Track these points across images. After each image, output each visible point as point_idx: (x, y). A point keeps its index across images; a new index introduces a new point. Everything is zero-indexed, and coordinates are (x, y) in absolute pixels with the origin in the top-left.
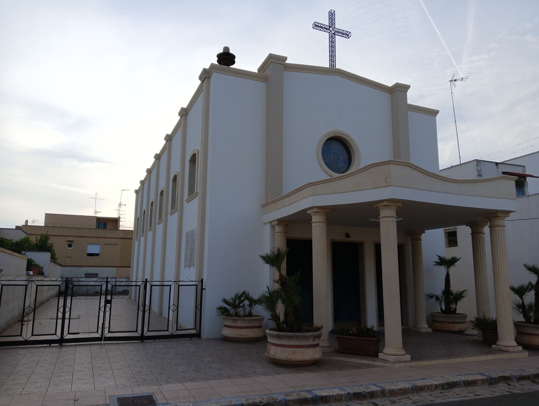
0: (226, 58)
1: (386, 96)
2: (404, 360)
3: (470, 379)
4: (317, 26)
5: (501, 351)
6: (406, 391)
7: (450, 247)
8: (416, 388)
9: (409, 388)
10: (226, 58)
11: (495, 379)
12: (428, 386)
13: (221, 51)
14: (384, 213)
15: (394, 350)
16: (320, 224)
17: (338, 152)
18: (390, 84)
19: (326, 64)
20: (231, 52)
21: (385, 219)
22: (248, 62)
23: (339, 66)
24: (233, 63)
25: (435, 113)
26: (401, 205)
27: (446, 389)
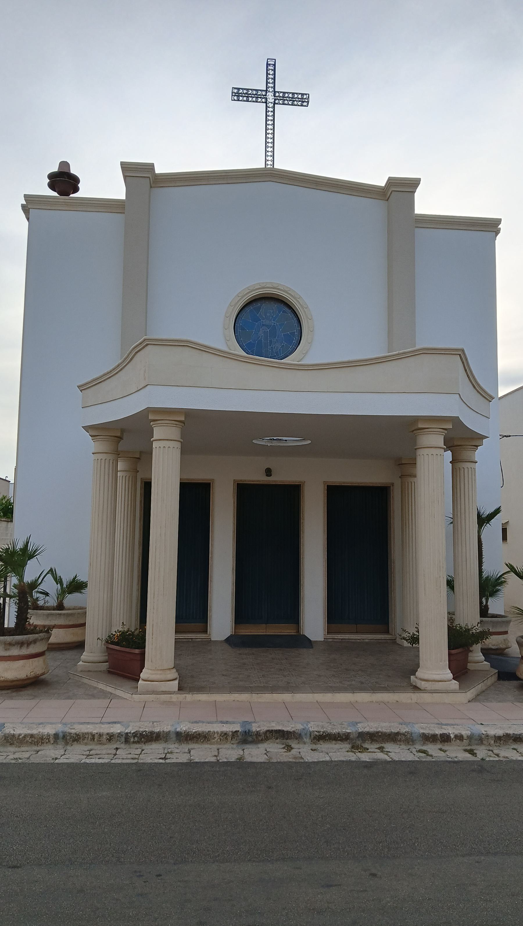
0: (64, 181)
1: (374, 207)
2: (164, 689)
3: (207, 730)
4: (240, 95)
5: (416, 688)
6: (42, 739)
7: (181, 484)
8: (64, 737)
9: (48, 735)
10: (64, 181)
11: (258, 734)
12: (93, 736)
13: (55, 169)
14: (158, 432)
15: (150, 671)
16: (100, 456)
17: (268, 324)
18: (382, 183)
19: (258, 163)
20: (71, 172)
21: (162, 444)
22: (102, 183)
23: (283, 163)
24: (76, 189)
25: (492, 226)
26: (182, 419)
27: (134, 742)
